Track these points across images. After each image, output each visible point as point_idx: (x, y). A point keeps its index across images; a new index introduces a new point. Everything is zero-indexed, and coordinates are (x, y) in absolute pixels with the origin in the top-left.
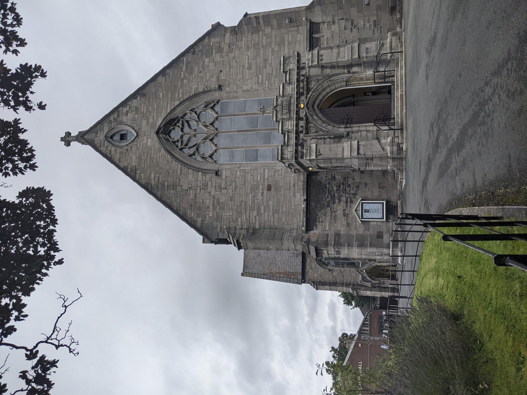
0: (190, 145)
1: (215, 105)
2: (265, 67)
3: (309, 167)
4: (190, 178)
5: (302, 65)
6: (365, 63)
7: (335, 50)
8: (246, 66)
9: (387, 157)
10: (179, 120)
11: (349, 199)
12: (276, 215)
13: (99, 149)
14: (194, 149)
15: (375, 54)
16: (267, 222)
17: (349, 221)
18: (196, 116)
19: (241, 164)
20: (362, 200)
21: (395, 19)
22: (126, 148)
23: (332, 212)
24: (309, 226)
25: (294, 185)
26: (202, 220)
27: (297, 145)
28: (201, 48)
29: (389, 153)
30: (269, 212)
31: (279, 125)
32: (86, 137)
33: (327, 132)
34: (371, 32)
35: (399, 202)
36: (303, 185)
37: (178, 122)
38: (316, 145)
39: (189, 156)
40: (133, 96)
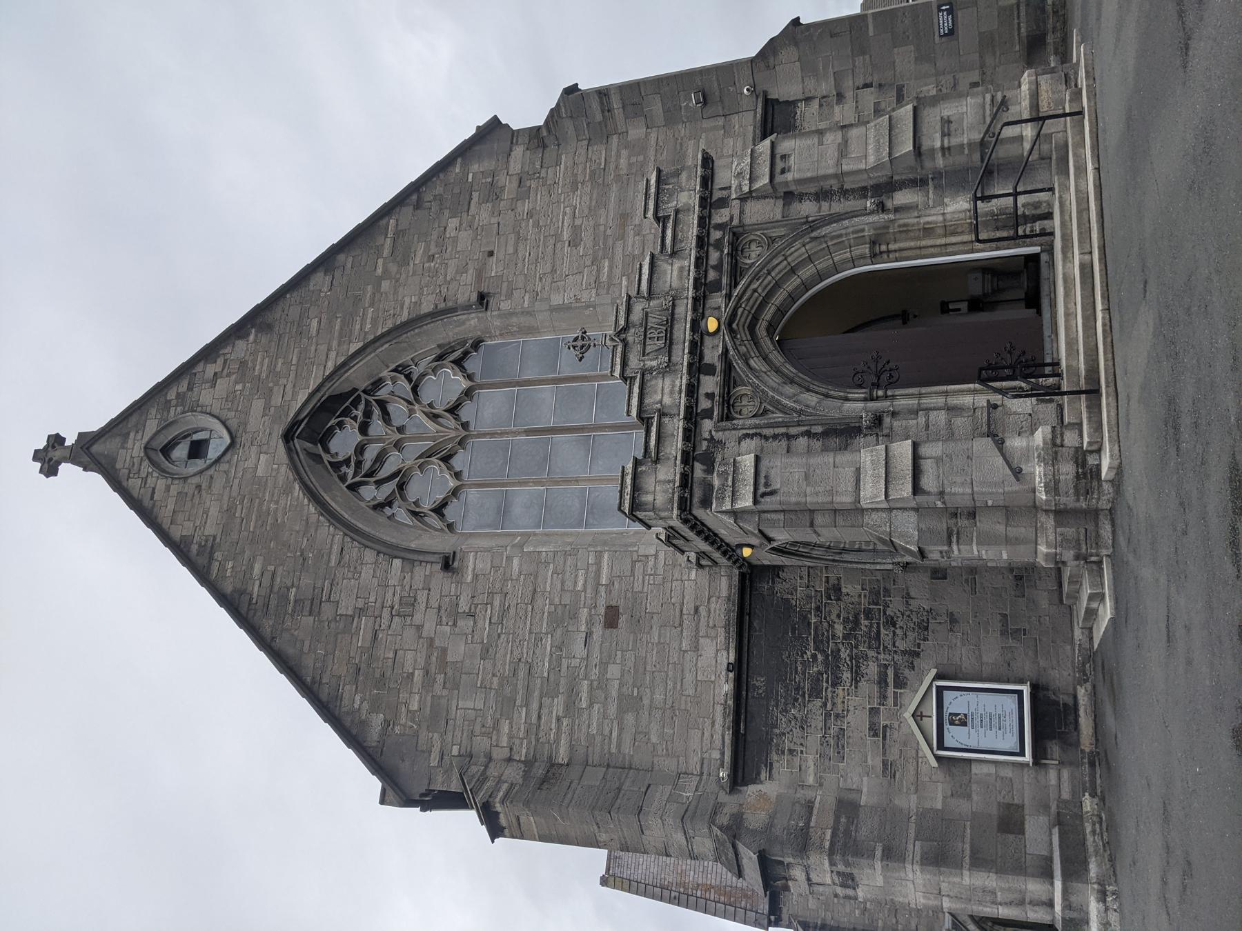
0: (384, 473)
1: (466, 354)
2: (623, 237)
3: (741, 546)
4: (366, 580)
5: (717, 195)
6: (938, 175)
7: (832, 139)
8: (566, 236)
9: (1035, 507)
10: (358, 398)
11: (890, 672)
13: (125, 484)
14: (391, 486)
15: (977, 136)
16: (599, 739)
17: (893, 755)
18: (408, 387)
19: (529, 535)
20: (939, 677)
22: (195, 480)
23: (827, 715)
24: (746, 761)
25: (697, 610)
26: (386, 723)
27: (688, 458)
28: (439, 190)
29: (1040, 487)
30: (605, 705)
31: (630, 392)
32: (96, 448)
33: (800, 412)
35: (1081, 692)
36: (728, 611)
37: (355, 404)
38: (758, 459)
39: (375, 507)
40: (237, 331)
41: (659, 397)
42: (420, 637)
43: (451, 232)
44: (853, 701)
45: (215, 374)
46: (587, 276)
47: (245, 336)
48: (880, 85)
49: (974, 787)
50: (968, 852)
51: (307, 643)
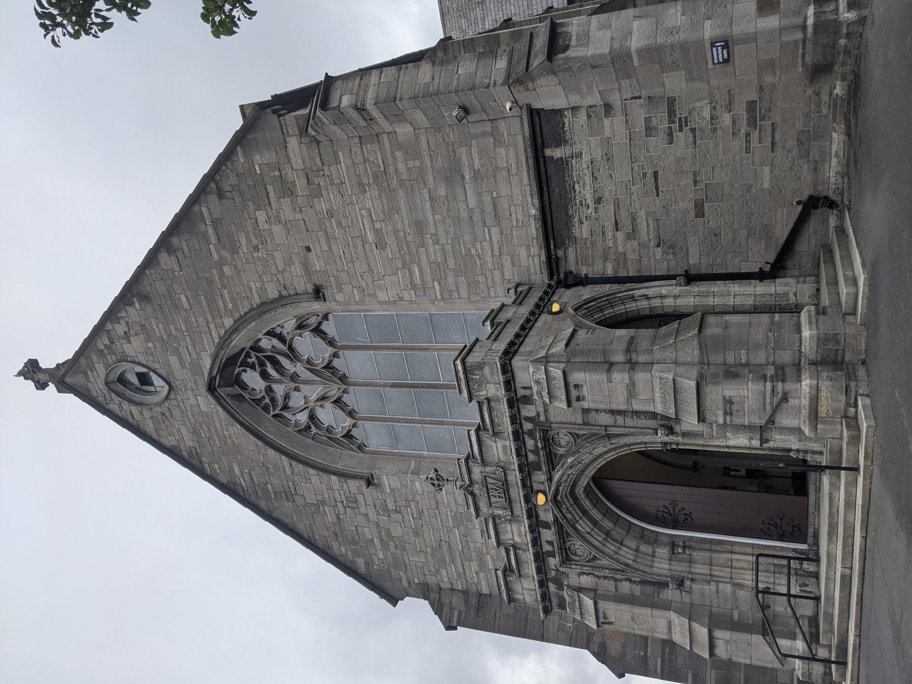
2: (423, 245)
5: (521, 393)
8: (370, 237)
21: (825, 97)
26: (367, 564)
28: (233, 180)
34: (738, 144)
37: (248, 355)
42: (369, 521)
43: (263, 225)
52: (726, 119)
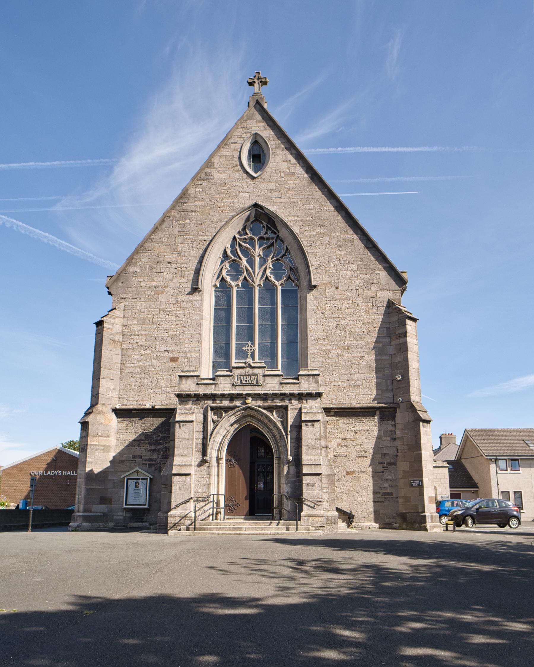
2: (339, 348)
10: (275, 234)
11: (154, 462)
12: (137, 370)
20: (150, 478)
21: (392, 520)
35: (147, 524)
37: (273, 232)
41: (222, 383)
42: (168, 282)
44: (144, 450)
45: (290, 161)
46: (321, 334)
47: (307, 172)
48: (397, 456)
49: (117, 489)
50: (92, 487)
51: (167, 233)
52: (386, 485)
